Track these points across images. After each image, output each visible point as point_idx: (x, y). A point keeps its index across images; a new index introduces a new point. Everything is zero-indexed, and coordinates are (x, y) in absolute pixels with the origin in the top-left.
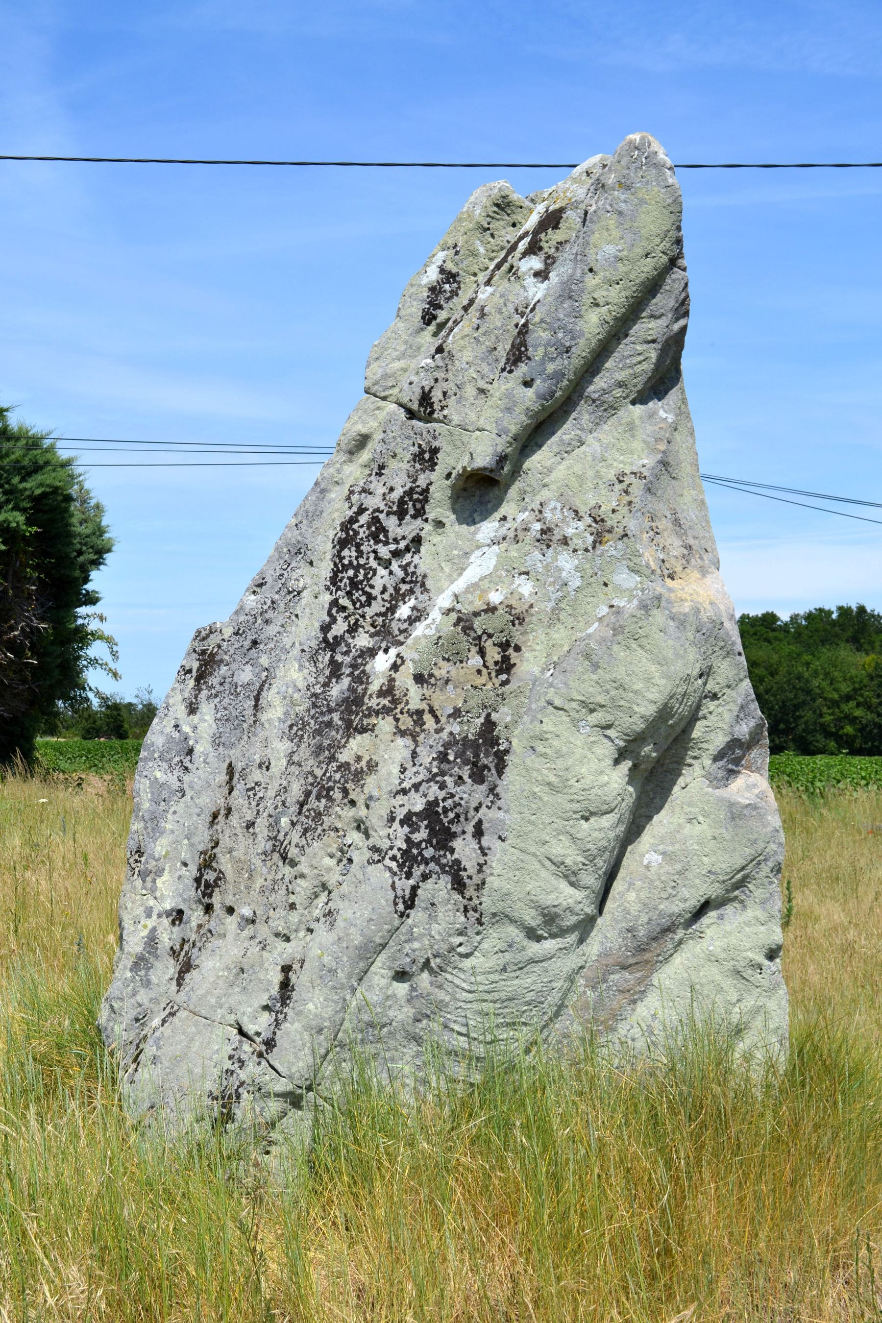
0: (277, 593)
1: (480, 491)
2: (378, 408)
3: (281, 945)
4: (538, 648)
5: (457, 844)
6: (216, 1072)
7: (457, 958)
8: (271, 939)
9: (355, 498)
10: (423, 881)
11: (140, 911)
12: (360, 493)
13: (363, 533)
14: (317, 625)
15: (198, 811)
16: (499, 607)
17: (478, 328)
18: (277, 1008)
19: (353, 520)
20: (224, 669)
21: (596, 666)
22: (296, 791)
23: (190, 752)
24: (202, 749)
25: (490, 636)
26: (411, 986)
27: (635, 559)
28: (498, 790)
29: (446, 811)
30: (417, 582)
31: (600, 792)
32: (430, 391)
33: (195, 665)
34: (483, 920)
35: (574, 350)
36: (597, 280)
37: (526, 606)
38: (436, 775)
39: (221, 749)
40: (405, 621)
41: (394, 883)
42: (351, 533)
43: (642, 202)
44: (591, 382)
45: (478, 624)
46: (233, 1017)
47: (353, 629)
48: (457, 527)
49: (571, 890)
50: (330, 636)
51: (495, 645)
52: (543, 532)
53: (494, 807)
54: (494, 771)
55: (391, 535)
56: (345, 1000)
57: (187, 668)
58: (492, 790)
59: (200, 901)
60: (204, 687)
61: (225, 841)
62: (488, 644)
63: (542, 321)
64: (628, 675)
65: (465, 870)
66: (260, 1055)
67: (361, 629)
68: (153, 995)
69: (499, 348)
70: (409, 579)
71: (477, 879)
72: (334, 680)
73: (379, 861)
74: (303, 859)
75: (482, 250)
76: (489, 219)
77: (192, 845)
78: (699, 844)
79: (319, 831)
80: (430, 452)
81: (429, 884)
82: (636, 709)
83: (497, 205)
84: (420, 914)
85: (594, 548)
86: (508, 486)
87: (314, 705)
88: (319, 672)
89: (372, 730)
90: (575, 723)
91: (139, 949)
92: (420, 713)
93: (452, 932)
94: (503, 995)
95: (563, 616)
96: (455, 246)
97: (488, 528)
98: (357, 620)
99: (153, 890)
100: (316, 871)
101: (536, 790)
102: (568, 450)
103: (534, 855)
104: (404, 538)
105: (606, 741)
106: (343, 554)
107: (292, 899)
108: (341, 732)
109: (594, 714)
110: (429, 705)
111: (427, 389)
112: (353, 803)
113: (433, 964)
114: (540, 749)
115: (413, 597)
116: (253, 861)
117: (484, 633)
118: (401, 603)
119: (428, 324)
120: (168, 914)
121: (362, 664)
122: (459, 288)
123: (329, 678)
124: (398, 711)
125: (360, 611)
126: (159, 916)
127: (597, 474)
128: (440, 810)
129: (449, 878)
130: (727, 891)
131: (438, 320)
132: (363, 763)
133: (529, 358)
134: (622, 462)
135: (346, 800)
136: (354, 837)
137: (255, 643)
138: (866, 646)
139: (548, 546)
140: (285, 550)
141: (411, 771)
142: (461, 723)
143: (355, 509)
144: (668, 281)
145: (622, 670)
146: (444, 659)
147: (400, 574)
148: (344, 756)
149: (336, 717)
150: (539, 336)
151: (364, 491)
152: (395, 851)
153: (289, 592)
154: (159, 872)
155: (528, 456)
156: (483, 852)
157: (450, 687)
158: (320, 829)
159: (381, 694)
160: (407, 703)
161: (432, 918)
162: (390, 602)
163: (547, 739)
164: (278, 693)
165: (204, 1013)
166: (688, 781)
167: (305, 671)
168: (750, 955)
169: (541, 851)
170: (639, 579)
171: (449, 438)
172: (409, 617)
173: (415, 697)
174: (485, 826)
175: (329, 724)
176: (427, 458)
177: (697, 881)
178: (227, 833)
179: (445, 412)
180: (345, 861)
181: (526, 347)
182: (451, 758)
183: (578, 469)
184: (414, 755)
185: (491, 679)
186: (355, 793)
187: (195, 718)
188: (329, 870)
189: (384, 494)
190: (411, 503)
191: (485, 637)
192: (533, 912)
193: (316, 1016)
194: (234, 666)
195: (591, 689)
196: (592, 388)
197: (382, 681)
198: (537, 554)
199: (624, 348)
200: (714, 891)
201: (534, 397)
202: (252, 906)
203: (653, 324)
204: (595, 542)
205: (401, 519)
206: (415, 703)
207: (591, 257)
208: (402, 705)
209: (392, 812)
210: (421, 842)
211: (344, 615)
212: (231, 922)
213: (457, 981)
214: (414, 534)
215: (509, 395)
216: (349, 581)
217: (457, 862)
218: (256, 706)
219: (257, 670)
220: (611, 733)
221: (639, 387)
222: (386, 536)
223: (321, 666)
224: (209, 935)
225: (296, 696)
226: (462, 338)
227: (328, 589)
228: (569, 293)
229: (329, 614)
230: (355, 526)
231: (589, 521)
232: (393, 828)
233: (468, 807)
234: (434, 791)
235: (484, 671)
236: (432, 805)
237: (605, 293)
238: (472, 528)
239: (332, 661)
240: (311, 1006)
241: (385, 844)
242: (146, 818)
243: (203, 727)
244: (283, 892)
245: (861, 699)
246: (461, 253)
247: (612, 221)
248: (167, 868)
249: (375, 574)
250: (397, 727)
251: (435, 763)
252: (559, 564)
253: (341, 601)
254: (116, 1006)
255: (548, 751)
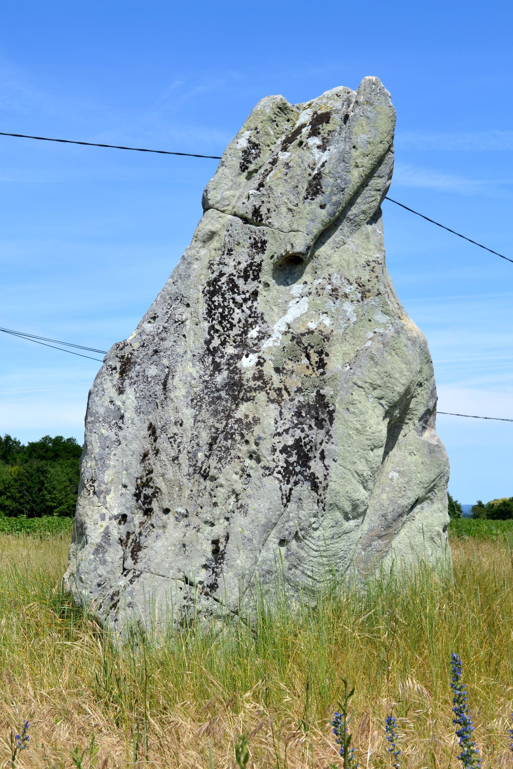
0: (166, 322)
1: (291, 266)
2: (220, 217)
3: (208, 528)
4: (338, 354)
5: (312, 463)
6: (176, 608)
7: (312, 531)
8: (202, 525)
9: (215, 267)
10: (295, 486)
11: (97, 516)
12: (218, 265)
13: (225, 287)
14: (202, 341)
15: (131, 453)
16: (315, 331)
17: (286, 174)
18: (213, 566)
19: (216, 280)
20: (138, 367)
21: (376, 364)
22: (205, 437)
23: (122, 417)
24: (129, 416)
25: (312, 347)
26: (288, 548)
27: (386, 307)
28: (331, 433)
29: (306, 444)
30: (258, 317)
31: (379, 435)
32: (259, 208)
33: (118, 365)
34: (326, 508)
35: (346, 190)
36: (358, 153)
37: (329, 331)
38: (297, 425)
39: (142, 415)
40: (256, 339)
41: (281, 486)
42: (217, 287)
43: (379, 113)
44: (350, 210)
45: (305, 340)
46: (182, 574)
47: (223, 343)
48: (277, 287)
49: (363, 491)
50: (211, 347)
51: (315, 352)
52: (333, 290)
53: (330, 443)
54: (328, 422)
55: (241, 290)
56: (256, 557)
57: (113, 367)
58: (327, 433)
59: (140, 508)
60: (126, 378)
61: (157, 469)
62: (311, 352)
63: (330, 172)
64: (392, 369)
65: (318, 478)
66: (207, 594)
67: (228, 344)
68: (109, 569)
69: (300, 187)
70: (253, 315)
71: (324, 484)
72: (217, 373)
73: (270, 475)
74: (221, 475)
75: (272, 133)
76: (275, 115)
77: (128, 474)
78: (415, 466)
79: (229, 459)
80: (261, 243)
81: (298, 488)
82: (396, 388)
83: (280, 108)
84: (293, 505)
85: (362, 300)
86: (306, 265)
87: (206, 387)
88: (206, 368)
89: (253, 400)
90: (367, 394)
91: (98, 540)
92: (280, 389)
93: (311, 515)
94: (330, 553)
95: (347, 337)
96: (256, 129)
97: (297, 288)
98: (225, 338)
99: (105, 503)
100: (229, 483)
101: (351, 433)
102: (337, 247)
103: (350, 470)
104: (248, 291)
105: (380, 406)
106: (213, 299)
107: (214, 500)
108: (229, 402)
109: (376, 391)
110: (284, 386)
111: (257, 207)
112: (247, 442)
113: (300, 534)
114: (352, 409)
115: (257, 326)
116: (181, 480)
117: (309, 345)
118: (250, 329)
119: (243, 171)
120: (116, 518)
121: (234, 363)
122: (260, 152)
123: (214, 371)
124: (268, 388)
125: (227, 333)
126: (110, 519)
127: (356, 261)
128: (303, 444)
129: (309, 484)
130: (427, 493)
131: (249, 170)
132: (250, 419)
133: (323, 193)
134: (366, 255)
135: (243, 440)
136: (251, 463)
137: (156, 352)
138: (11, 461)
139: (337, 298)
140: (168, 297)
141: (280, 423)
142: (304, 395)
143: (216, 274)
144: (387, 158)
145: (389, 366)
146: (289, 359)
147: (248, 312)
148: (238, 415)
149: (223, 394)
150: (327, 182)
151: (220, 263)
152: (279, 468)
153: (176, 322)
154: (108, 492)
155: (318, 248)
156: (326, 468)
157: (294, 375)
158: (229, 457)
159: (255, 379)
160: (272, 384)
161: (300, 507)
162: (243, 328)
163: (355, 404)
164: (180, 380)
165: (161, 573)
166: (406, 432)
167: (197, 367)
168: (437, 528)
169: (353, 468)
170: (388, 318)
171: (272, 235)
172: (258, 337)
173: (276, 380)
174: (326, 453)
175: (219, 398)
176: (259, 246)
177: (415, 487)
178: (158, 464)
179: (270, 220)
180: (245, 476)
181: (320, 186)
182: (304, 415)
183: (345, 256)
184: (281, 413)
185: (314, 371)
186: (248, 436)
187: (123, 397)
188: (236, 481)
189: (235, 266)
190: (251, 272)
191: (309, 348)
192: (349, 503)
193: (242, 567)
194: (144, 366)
195: (375, 377)
196: (350, 213)
197: (253, 372)
198: (331, 303)
199: (366, 193)
200: (420, 492)
201: (326, 214)
202: (184, 507)
203: (379, 181)
204: (362, 297)
205: (246, 280)
206: (277, 384)
207: (354, 140)
208: (270, 385)
209: (273, 446)
210: (293, 463)
211: (218, 335)
212: (170, 519)
213: (311, 545)
214: (253, 290)
215: (312, 212)
216: (218, 315)
217: (313, 474)
218: (165, 389)
219: (161, 368)
220: (383, 402)
221: (371, 215)
222: (238, 290)
223: (207, 364)
224: (151, 527)
225: (193, 382)
226: (277, 179)
227: (206, 319)
228: (343, 158)
229: (209, 333)
230: (219, 283)
231: (356, 285)
232: (276, 455)
233: (316, 443)
234: (298, 433)
235: (310, 367)
236: (298, 441)
237: (361, 161)
238: (288, 288)
239: (214, 362)
240: (238, 562)
241: (272, 465)
242: (97, 458)
243: (128, 402)
244: (207, 495)
245: (8, 494)
246: (261, 133)
247: (364, 122)
248: (113, 489)
249: (234, 311)
250: (268, 398)
251: (294, 418)
252: (345, 308)
253: (216, 327)
254: (83, 577)
255: (356, 411)
